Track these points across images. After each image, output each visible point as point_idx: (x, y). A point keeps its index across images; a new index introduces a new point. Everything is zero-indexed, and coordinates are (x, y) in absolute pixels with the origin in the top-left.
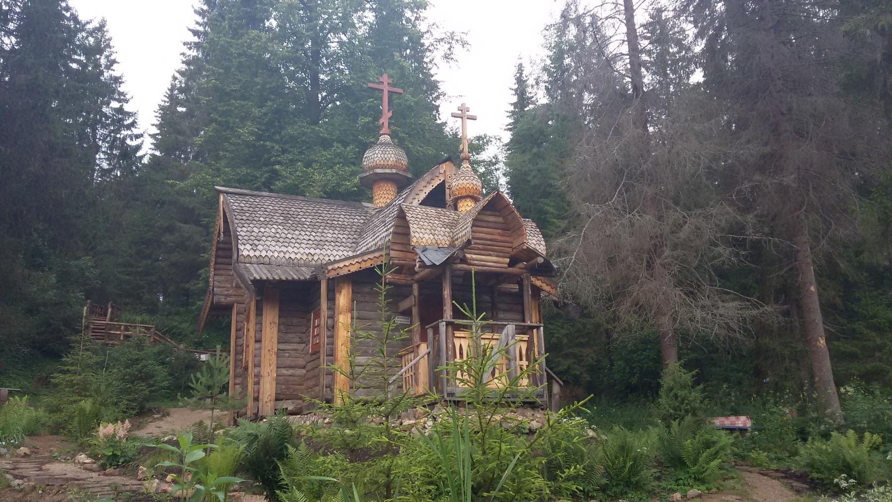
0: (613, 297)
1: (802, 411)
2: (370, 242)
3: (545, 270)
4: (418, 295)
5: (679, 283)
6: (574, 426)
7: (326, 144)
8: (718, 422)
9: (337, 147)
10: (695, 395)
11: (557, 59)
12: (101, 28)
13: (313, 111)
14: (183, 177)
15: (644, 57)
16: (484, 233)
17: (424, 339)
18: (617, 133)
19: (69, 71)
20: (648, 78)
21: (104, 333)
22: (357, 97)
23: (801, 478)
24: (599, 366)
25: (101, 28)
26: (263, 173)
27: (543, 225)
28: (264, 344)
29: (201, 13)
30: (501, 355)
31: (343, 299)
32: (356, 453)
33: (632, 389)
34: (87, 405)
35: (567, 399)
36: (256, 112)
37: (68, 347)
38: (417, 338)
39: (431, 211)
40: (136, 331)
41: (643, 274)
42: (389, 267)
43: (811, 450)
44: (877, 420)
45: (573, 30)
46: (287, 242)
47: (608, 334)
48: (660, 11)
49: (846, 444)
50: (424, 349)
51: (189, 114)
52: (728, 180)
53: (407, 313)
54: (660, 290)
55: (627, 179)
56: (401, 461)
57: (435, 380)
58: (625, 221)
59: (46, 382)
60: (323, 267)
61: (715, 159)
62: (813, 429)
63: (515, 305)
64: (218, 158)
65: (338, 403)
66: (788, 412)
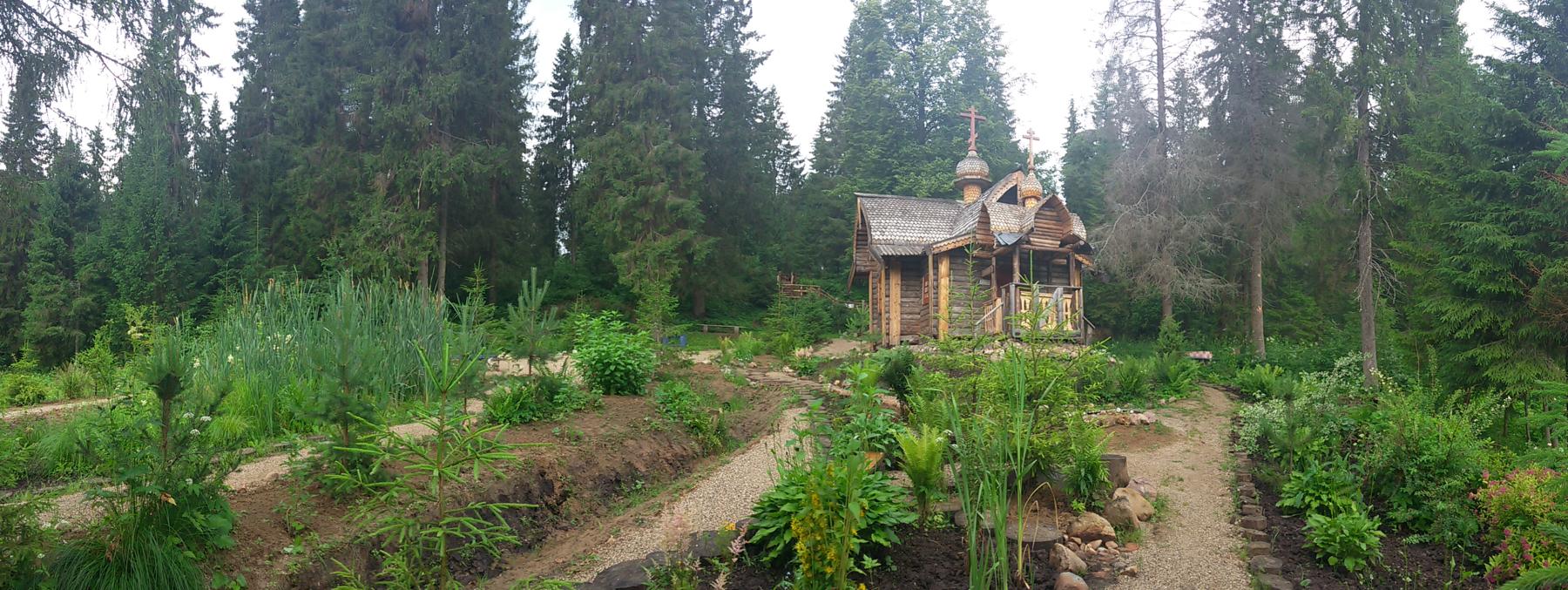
0: (1133, 271)
1: (1243, 351)
2: (962, 228)
3: (1085, 250)
4: (995, 266)
5: (1177, 264)
6: (1100, 355)
7: (930, 158)
8: (1192, 355)
9: (938, 160)
10: (1180, 337)
11: (1103, 96)
12: (773, 92)
13: (921, 135)
14: (832, 187)
15: (1169, 103)
16: (1043, 223)
17: (999, 295)
18: (1145, 155)
19: (756, 124)
20: (1170, 119)
21: (790, 291)
22: (951, 123)
23: (1235, 391)
24: (1119, 315)
25: (773, 92)
26: (887, 181)
27: (1086, 219)
28: (892, 297)
29: (839, 70)
30: (1053, 308)
31: (944, 267)
32: (953, 371)
33: (1142, 331)
34: (786, 336)
35: (1099, 336)
36: (880, 138)
37: (771, 300)
38: (994, 295)
39: (1005, 206)
40: (810, 289)
41: (1155, 255)
42: (976, 246)
43: (1243, 375)
44: (1284, 359)
45: (1115, 79)
46: (905, 229)
47: (1129, 294)
48: (1183, 71)
49: (1264, 373)
50: (999, 302)
51: (834, 142)
52: (1216, 198)
53: (988, 278)
54: (1164, 266)
55: (1147, 189)
56: (983, 378)
57: (1007, 326)
58: (1146, 218)
59: (760, 322)
60: (930, 246)
61: (1208, 182)
62: (1247, 363)
63: (1064, 273)
64: (855, 173)
65: (942, 338)
66: (1235, 351)
